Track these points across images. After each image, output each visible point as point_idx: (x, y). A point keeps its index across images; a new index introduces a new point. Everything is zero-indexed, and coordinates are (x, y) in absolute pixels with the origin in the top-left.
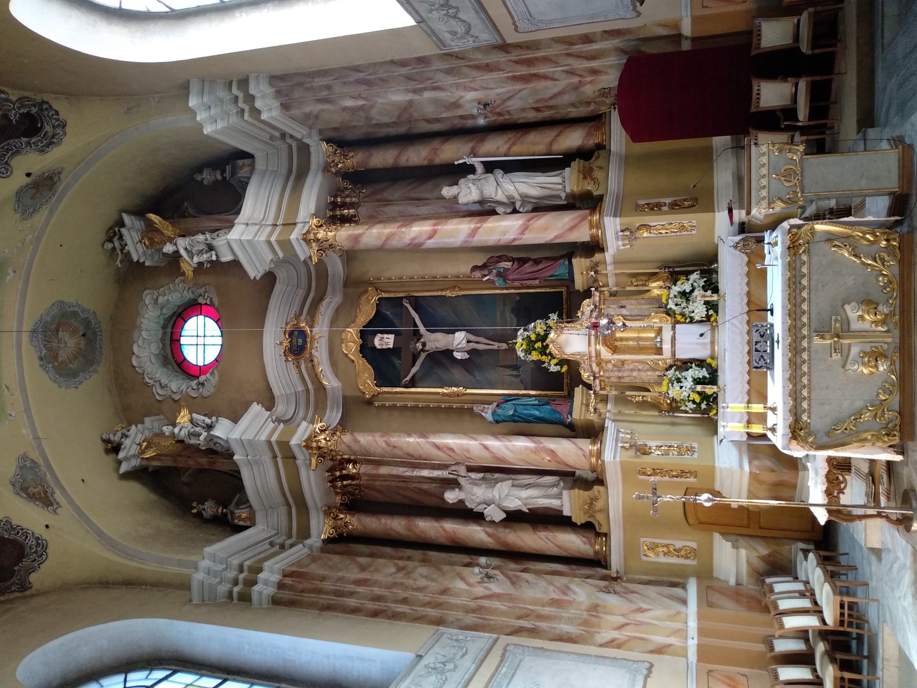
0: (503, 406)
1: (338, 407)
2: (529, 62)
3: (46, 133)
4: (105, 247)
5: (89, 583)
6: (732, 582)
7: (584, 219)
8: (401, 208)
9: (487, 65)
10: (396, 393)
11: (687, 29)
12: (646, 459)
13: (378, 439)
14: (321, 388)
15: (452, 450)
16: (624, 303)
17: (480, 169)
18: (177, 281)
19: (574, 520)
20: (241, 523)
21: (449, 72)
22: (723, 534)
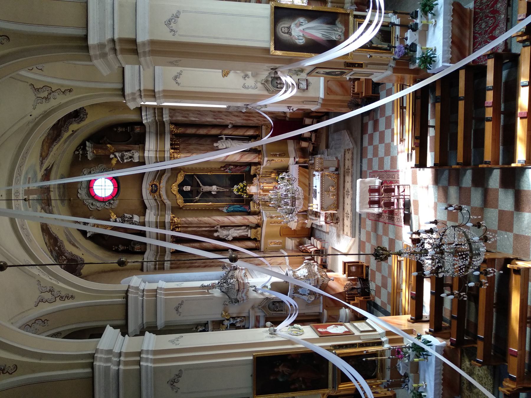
0: (229, 207)
1: (170, 209)
2: (249, 116)
3: (81, 117)
4: (76, 153)
5: (99, 272)
6: (291, 249)
7: (257, 157)
8: (195, 147)
9: (237, 115)
10: (195, 205)
11: (288, 116)
12: (273, 219)
13: (195, 219)
14: (164, 204)
15: (219, 220)
16: (265, 179)
17: (224, 139)
18: (99, 166)
19: (251, 238)
20: (137, 250)
21: (226, 115)
22: (289, 237)
